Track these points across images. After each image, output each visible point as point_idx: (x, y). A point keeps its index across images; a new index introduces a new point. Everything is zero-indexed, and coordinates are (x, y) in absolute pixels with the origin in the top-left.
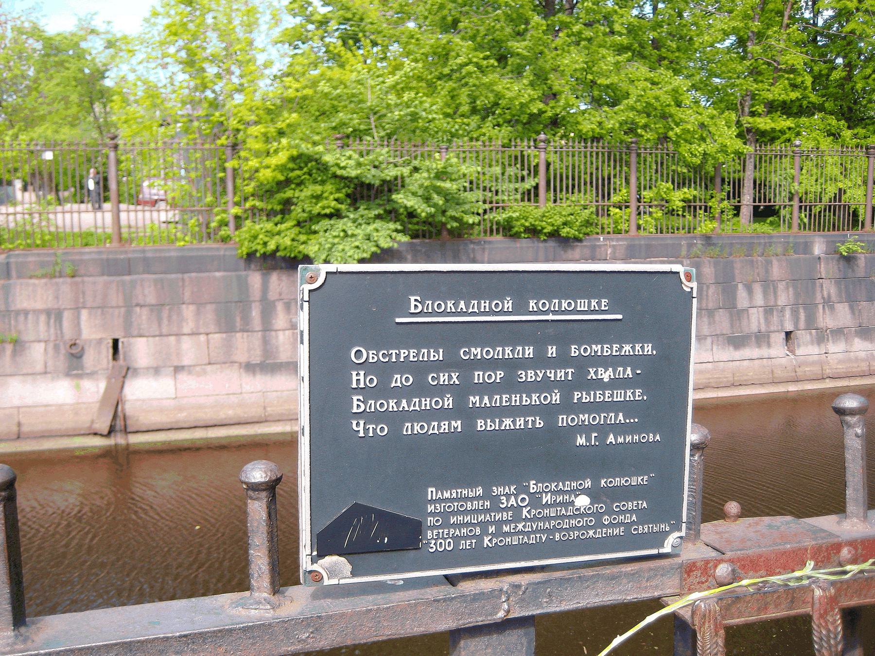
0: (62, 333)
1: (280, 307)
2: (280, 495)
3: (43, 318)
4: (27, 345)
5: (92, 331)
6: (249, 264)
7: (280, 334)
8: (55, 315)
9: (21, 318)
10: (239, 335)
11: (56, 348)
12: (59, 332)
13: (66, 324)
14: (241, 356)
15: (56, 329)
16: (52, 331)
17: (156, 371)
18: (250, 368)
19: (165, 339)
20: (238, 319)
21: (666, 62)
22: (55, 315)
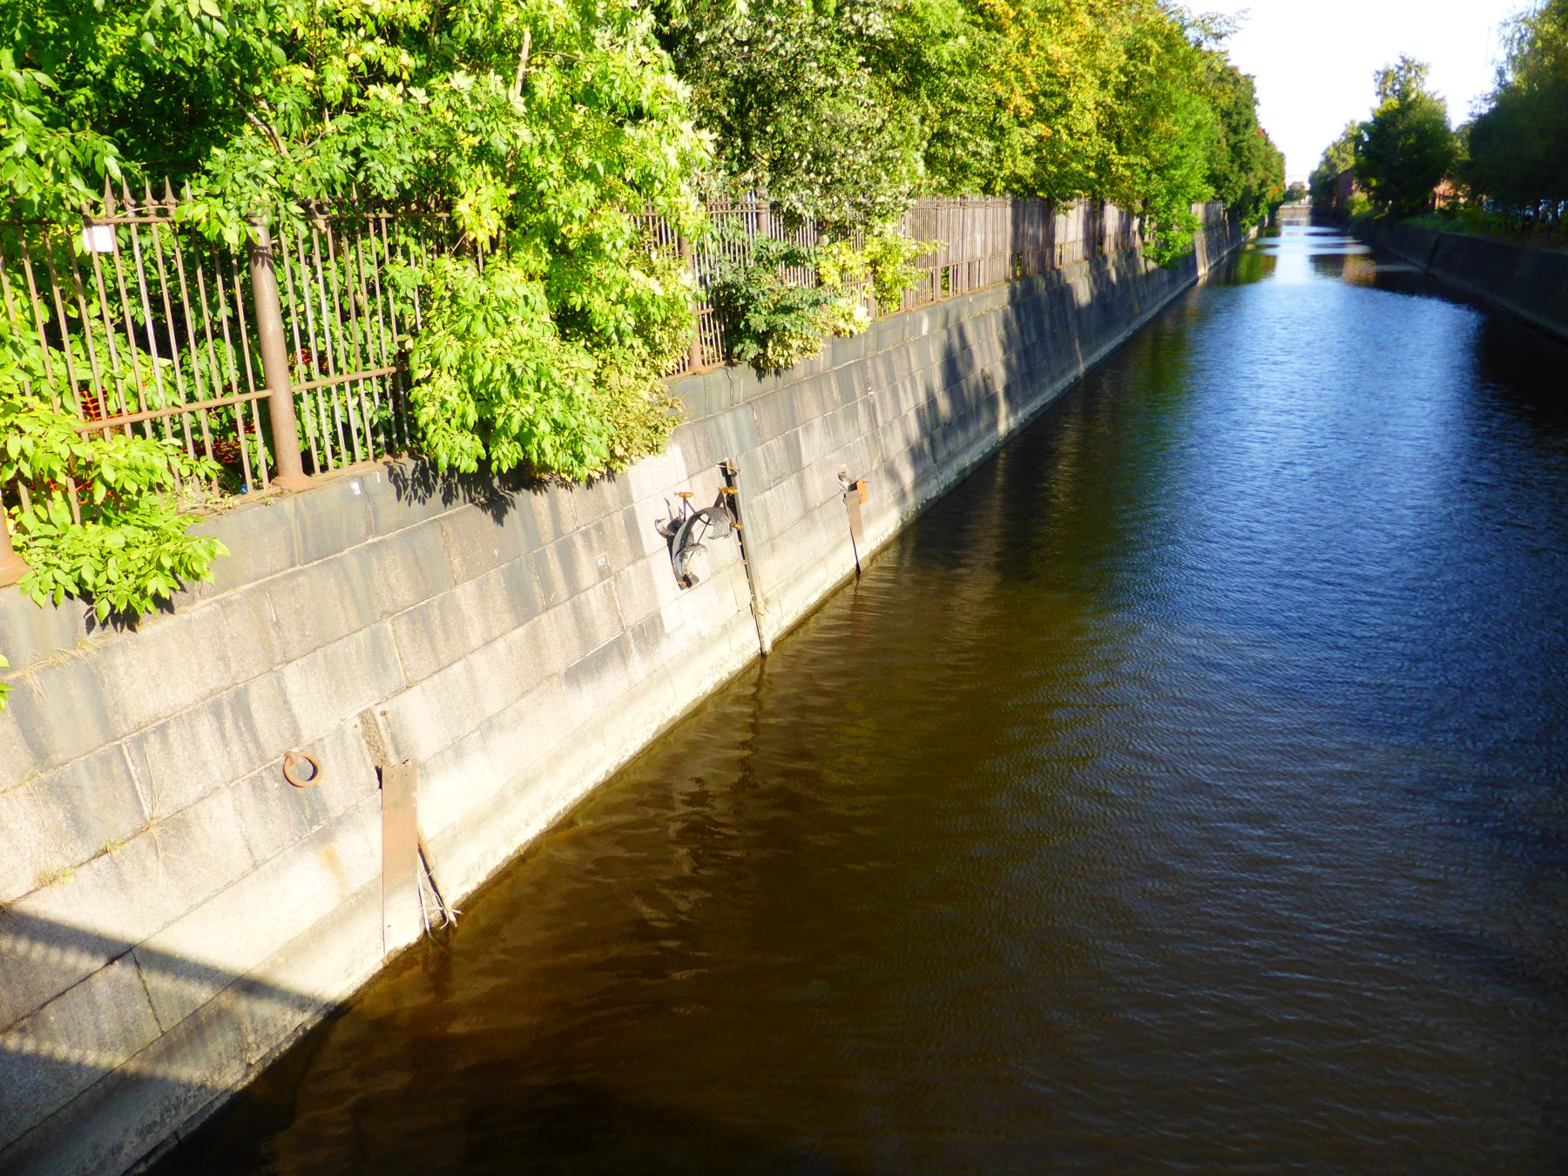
0: (258, 746)
1: (579, 543)
2: (92, 1002)
3: (206, 726)
4: (191, 814)
5: (319, 709)
6: (1419, 149)
7: (590, 592)
8: (231, 708)
9: (153, 746)
10: (544, 617)
11: (257, 785)
12: (251, 746)
13: (262, 717)
14: (558, 662)
15: (244, 743)
16: (236, 748)
17: (457, 750)
18: (576, 674)
19: (448, 671)
20: (537, 589)
21: (630, 174)
22: (231, 708)
